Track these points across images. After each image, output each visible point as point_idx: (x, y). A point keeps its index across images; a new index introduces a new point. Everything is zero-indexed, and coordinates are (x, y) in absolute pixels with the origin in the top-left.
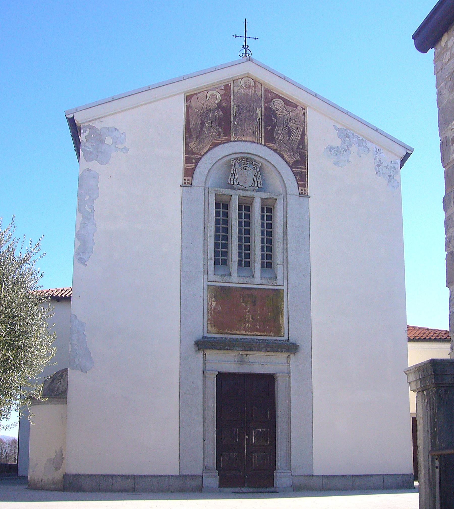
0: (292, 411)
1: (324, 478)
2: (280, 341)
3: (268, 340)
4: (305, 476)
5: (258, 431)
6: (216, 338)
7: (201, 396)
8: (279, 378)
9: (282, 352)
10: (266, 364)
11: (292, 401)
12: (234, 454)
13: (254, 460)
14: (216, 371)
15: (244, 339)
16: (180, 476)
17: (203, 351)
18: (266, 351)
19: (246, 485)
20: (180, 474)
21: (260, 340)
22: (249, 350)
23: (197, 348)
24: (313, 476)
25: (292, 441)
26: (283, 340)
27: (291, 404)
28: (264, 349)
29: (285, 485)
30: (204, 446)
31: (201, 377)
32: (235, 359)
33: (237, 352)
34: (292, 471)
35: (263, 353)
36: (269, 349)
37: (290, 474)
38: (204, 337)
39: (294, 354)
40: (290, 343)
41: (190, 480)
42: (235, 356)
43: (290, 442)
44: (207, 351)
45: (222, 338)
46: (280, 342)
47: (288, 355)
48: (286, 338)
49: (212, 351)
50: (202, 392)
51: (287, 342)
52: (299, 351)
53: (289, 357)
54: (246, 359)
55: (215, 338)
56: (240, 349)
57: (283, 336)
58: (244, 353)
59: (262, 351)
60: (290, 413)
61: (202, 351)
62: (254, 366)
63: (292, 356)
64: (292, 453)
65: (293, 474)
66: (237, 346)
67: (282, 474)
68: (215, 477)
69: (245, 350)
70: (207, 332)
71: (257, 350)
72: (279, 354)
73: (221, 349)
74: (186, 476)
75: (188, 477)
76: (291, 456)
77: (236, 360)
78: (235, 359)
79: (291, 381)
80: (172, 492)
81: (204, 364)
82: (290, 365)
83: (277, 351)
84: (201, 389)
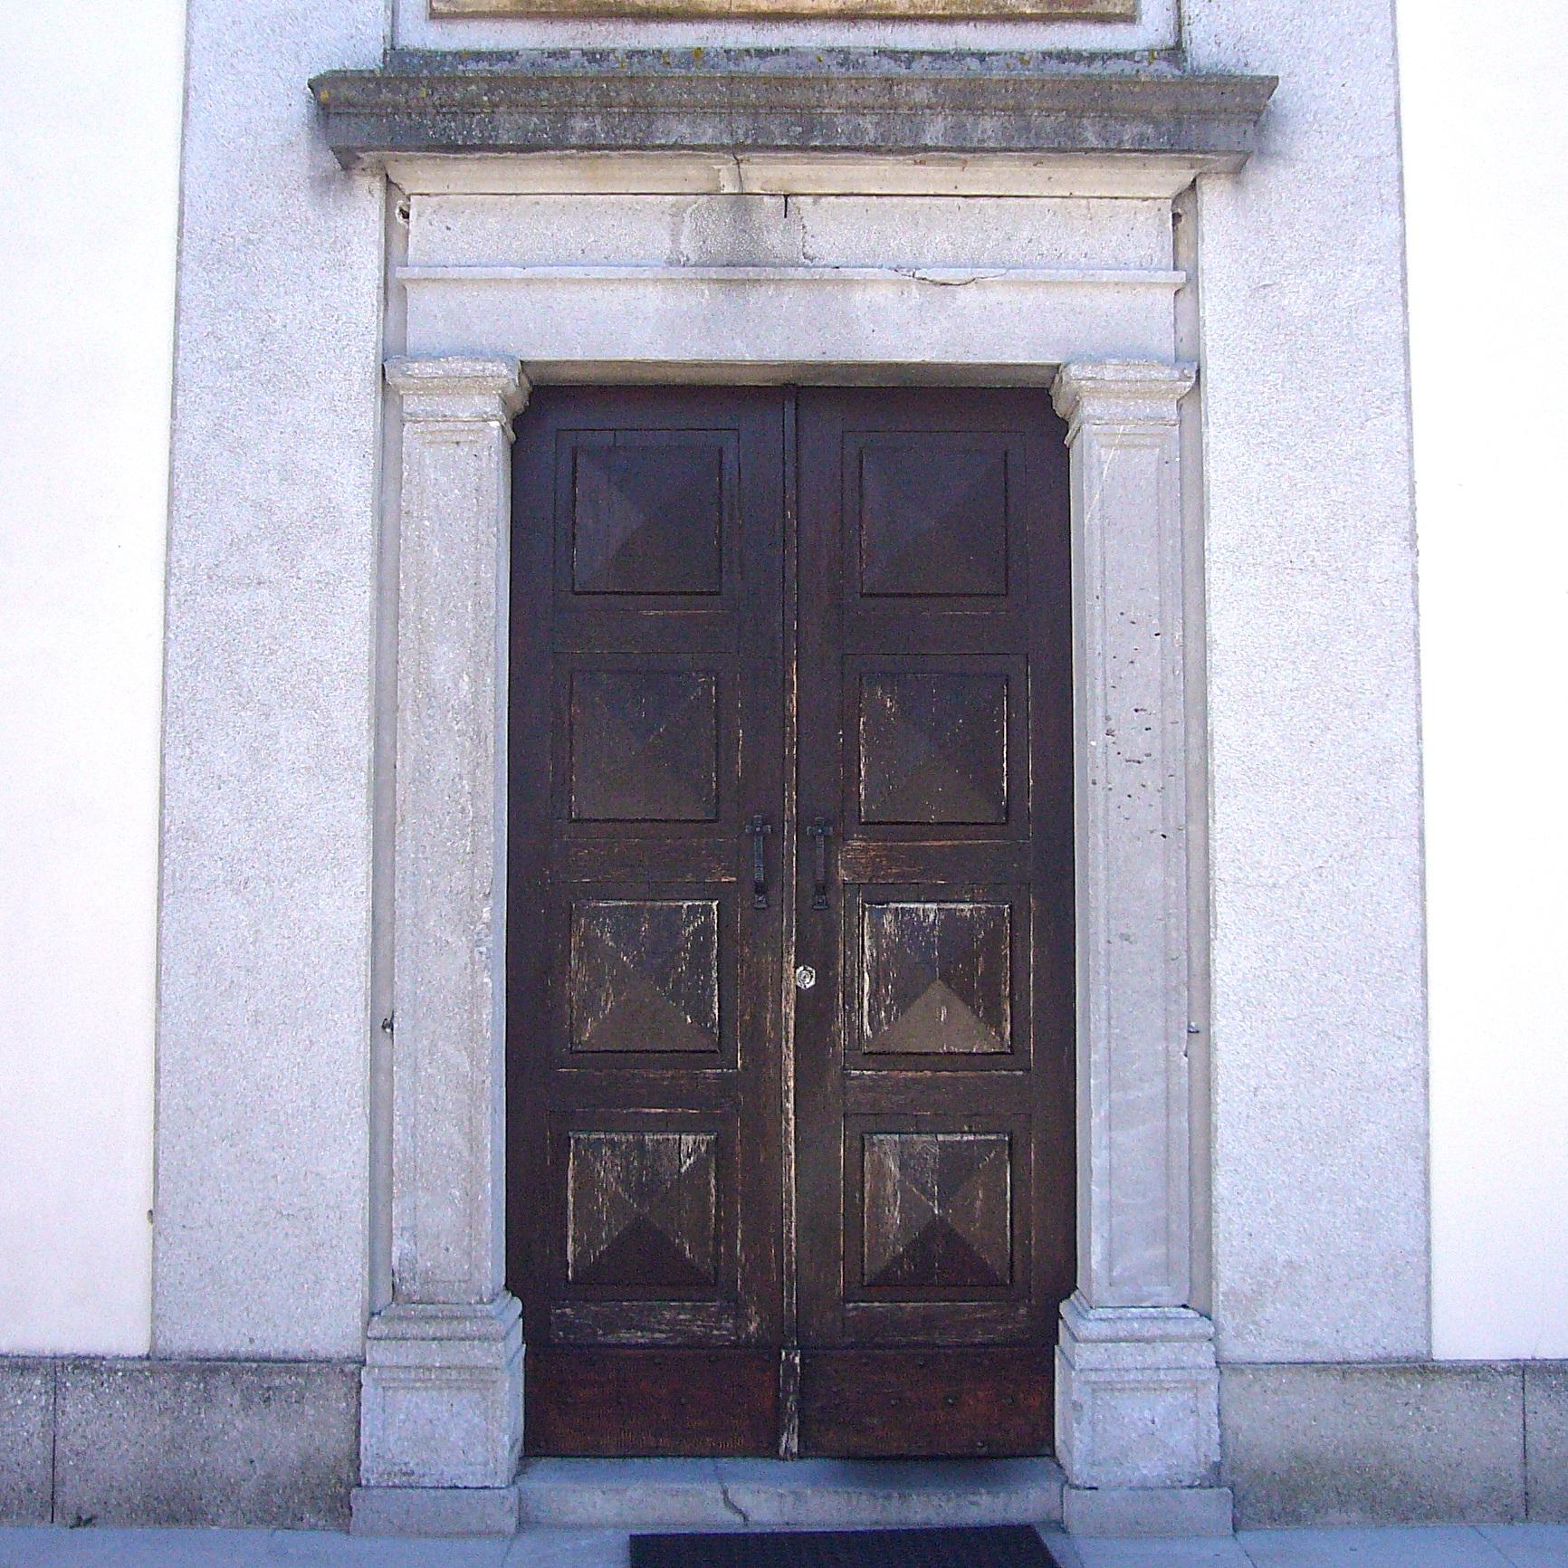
0: (1225, 725)
1: (1535, 1396)
2: (1093, 57)
3: (981, 57)
4: (1345, 1368)
5: (909, 924)
6: (510, 56)
7: (359, 598)
8: (1090, 408)
9: (1111, 151)
10: (964, 274)
11: (1222, 626)
12: (688, 1139)
13: (873, 1199)
14: (500, 356)
15: (762, 53)
16: (156, 1363)
17: (389, 183)
18: (962, 149)
19: (790, 1441)
20: (161, 1342)
21: (913, 55)
22: (802, 147)
23: (329, 161)
24: (1424, 1368)
25: (1225, 1026)
26: (1128, 56)
27: (1214, 658)
28: (934, 132)
29: (1150, 1467)
30: (379, 1069)
31: (366, 421)
32: (675, 241)
33: (692, 172)
34: (1221, 1314)
35: (935, 176)
36: (988, 127)
37: (1205, 1356)
38: (395, 54)
39: (1237, 171)
40: (1195, 73)
41: (247, 1402)
42: (677, 213)
43: (1199, 1033)
44: (420, 176)
45: (563, 54)
46: (1097, 68)
47: (1170, 192)
48: (1151, 30)
49: (465, 174)
50: (363, 560)
51: (1163, 66)
52: (1279, 142)
53: (1183, 207)
54: (775, 240)
55: (500, 56)
56: (708, 134)
57: (1130, 18)
58: (764, 173)
59: (916, 150)
60: (1206, 745)
61: (378, 185)
62: (858, 296)
63: (1215, 199)
64: (1228, 1141)
65: (1236, 1350)
66: (681, 110)
67: (1128, 1355)
68: (478, 1377)
69: (766, 147)
70: (424, 13)
71: (871, 135)
72: (1090, 178)
73: (527, 147)
74: (209, 1367)
75: (225, 1375)
76: (1209, 1166)
77: (688, 247)
78: (675, 241)
79: (1210, 434)
80: (80, 1522)
81: (392, 292)
82: (1193, 281)
83: (1066, 147)
84: (361, 526)
